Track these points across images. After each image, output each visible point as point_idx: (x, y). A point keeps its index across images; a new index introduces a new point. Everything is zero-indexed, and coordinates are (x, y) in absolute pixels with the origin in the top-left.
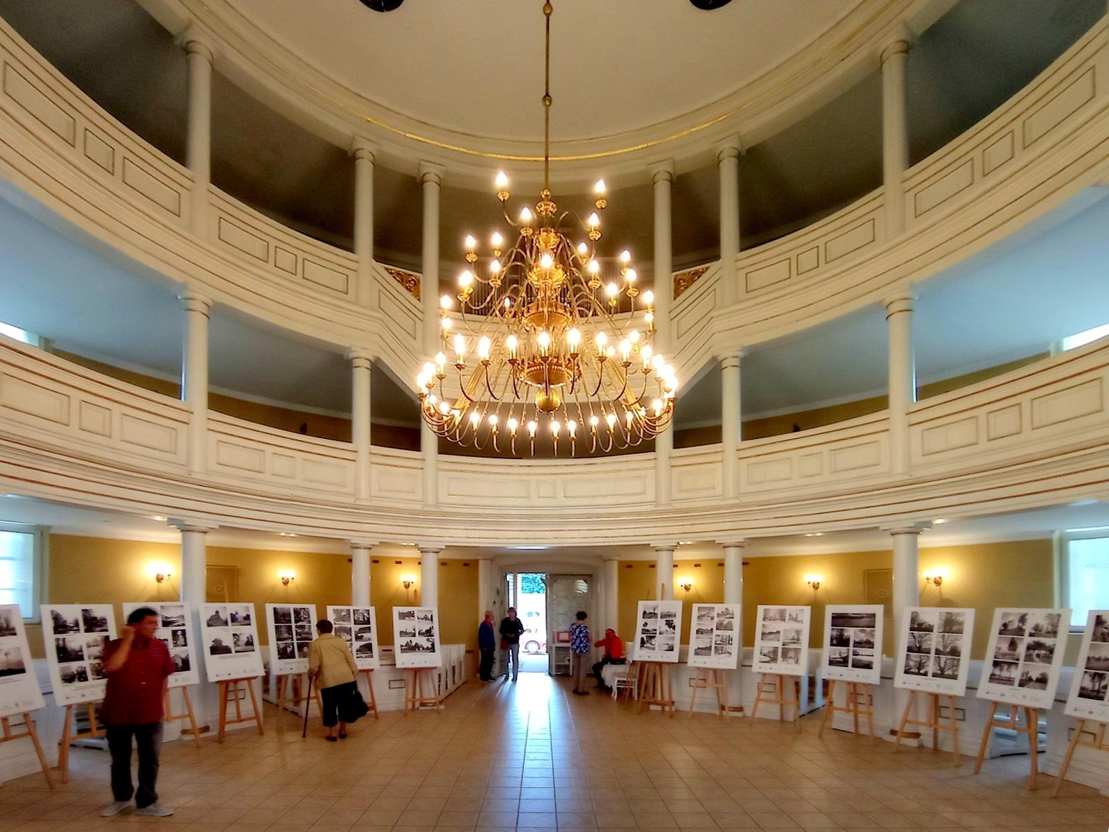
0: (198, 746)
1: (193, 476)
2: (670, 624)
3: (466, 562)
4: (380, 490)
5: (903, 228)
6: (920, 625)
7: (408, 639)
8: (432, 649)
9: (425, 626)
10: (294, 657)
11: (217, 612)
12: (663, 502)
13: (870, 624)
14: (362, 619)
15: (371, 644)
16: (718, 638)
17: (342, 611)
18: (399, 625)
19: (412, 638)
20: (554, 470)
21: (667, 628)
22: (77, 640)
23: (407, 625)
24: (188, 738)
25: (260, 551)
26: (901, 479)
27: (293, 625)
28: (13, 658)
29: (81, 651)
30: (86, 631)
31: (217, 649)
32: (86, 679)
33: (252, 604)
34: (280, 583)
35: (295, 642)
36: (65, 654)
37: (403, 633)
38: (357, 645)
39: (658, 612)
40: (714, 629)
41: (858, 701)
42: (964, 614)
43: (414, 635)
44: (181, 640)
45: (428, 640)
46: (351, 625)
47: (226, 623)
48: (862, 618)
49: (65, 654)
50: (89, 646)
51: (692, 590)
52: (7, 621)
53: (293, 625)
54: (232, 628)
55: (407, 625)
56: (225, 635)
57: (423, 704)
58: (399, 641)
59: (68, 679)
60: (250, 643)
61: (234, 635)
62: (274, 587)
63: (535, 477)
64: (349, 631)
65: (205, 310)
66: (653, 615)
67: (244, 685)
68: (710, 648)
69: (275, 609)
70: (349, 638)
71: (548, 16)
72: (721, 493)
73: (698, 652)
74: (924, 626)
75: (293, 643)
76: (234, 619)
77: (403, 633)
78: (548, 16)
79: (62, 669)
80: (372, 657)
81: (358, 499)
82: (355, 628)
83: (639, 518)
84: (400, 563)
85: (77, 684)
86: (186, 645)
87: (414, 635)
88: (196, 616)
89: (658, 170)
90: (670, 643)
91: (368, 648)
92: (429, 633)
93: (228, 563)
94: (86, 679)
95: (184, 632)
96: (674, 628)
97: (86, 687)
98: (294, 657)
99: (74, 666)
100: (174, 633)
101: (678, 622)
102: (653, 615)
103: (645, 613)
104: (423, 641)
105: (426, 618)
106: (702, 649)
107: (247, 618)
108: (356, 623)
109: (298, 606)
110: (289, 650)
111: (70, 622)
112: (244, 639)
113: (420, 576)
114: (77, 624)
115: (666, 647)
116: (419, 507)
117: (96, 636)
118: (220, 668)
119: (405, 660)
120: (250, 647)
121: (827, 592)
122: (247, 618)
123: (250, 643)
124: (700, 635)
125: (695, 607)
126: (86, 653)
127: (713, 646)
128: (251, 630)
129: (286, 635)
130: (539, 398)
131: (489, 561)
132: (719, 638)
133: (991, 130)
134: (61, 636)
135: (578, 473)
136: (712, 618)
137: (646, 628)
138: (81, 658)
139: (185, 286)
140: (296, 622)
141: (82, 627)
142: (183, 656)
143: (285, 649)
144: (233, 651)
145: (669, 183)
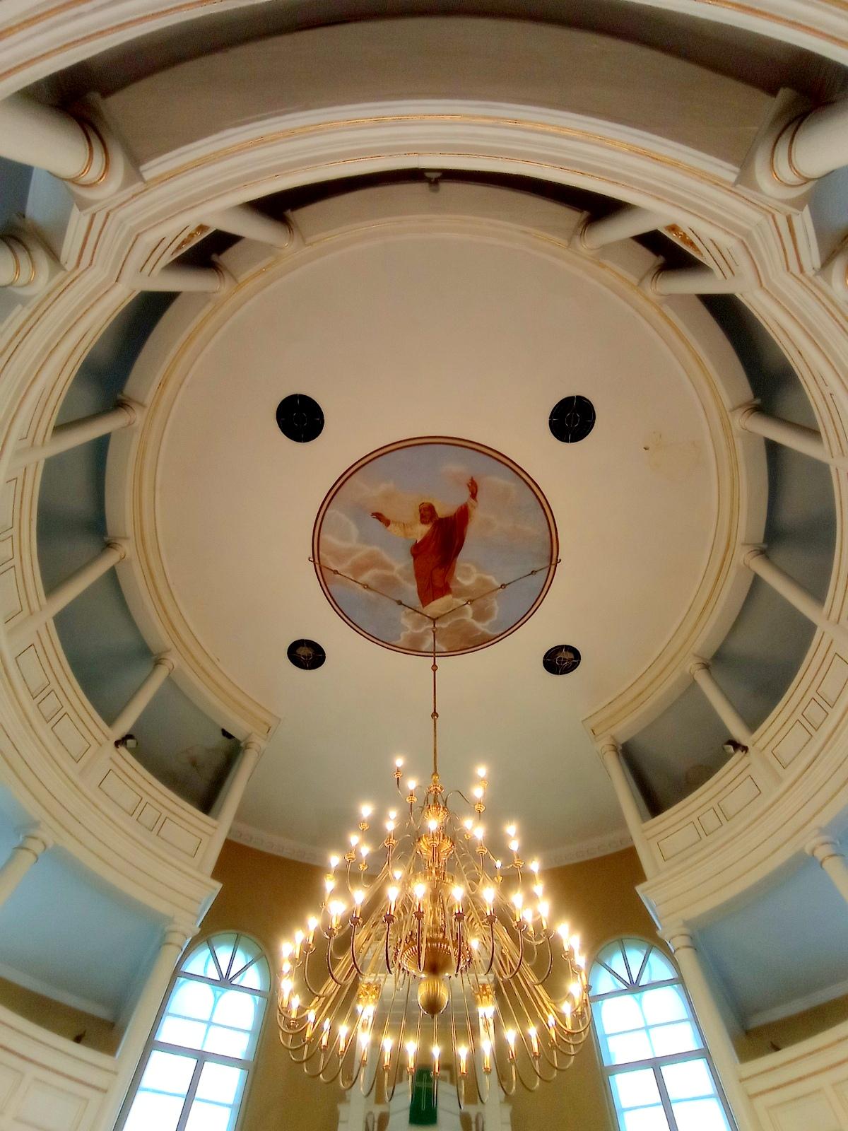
5: (779, 780)
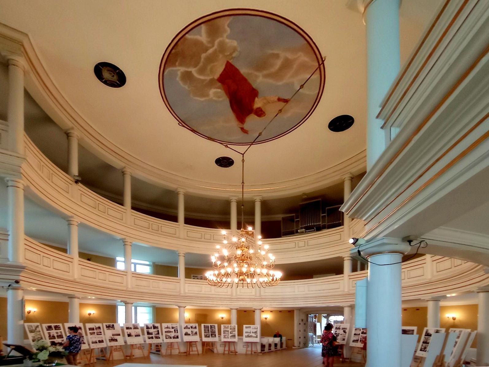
0: (180, 356)
1: (181, 295)
2: (344, 332)
3: (405, 309)
4: (240, 293)
6: (428, 334)
7: (248, 334)
8: (257, 337)
9: (255, 331)
10: (209, 337)
11: (187, 326)
12: (346, 291)
13: (412, 333)
14: (232, 328)
15: (235, 335)
16: (362, 337)
17: (226, 326)
18: (245, 330)
19: (250, 334)
20: (304, 283)
21: (343, 333)
22: (151, 331)
23: (248, 330)
24: (179, 354)
25: (214, 310)
26: (451, 274)
27: (210, 329)
28: (138, 333)
29: (152, 333)
30: (154, 329)
31: (186, 334)
32: (153, 338)
33: (217, 325)
34: (221, 318)
35: (210, 333)
36: (148, 333)
37: (246, 332)
38: (230, 335)
39: (341, 327)
40: (361, 333)
41: (197, 352)
42: (442, 330)
43: (250, 333)
44: (176, 332)
45: (255, 334)
46: (229, 329)
47: (189, 328)
48: (410, 331)
49: (148, 333)
50: (154, 332)
51: (456, 321)
52: (137, 327)
53: (210, 329)
54: (191, 330)
55: (248, 330)
56: (189, 331)
57: (231, 352)
58: (245, 334)
59: (149, 338)
60: (196, 333)
61: (192, 331)
62: (218, 320)
63: (297, 285)
64: (228, 331)
65: (183, 255)
66: (339, 328)
67: (194, 343)
68: (358, 340)
69: (204, 325)
70: (228, 333)
71: (243, 162)
72: (230, 294)
73: (354, 341)
74: (429, 334)
75: (209, 334)
76: (192, 327)
77: (246, 332)
78: (243, 162)
79: (148, 336)
80: (235, 338)
81: (232, 296)
82: (230, 331)
83: (251, 300)
84: (263, 312)
85: (151, 339)
86: (178, 333)
87: (250, 333)
88: (181, 327)
89: (345, 177)
90: (344, 338)
91: (234, 336)
92: (256, 332)
93: (204, 313)
94: (153, 338)
95: (177, 330)
96: (346, 333)
97: (153, 340)
98: (209, 337)
99: (151, 336)
100: (175, 330)
101: (347, 331)
102: (339, 328)
103: (336, 328)
104: (254, 335)
105: (255, 328)
106: (355, 340)
107: (196, 327)
108: (230, 329)
109: (211, 325)
110: (208, 335)
111: (150, 327)
112: (194, 332)
113: (261, 316)
114: (151, 327)
115: (342, 339)
116: (253, 297)
117: (156, 330)
118: (187, 339)
119: (246, 340)
120: (196, 334)
121: (460, 321)
122: (196, 327)
123: (196, 333)
124: (355, 336)
125: (222, 326)
126: (153, 333)
127: (360, 339)
128: (195, 331)
129: (207, 332)
130: (237, 270)
131: (298, 311)
132: (362, 337)
133: (138, 216)
134: (148, 330)
135: (289, 285)
136: (360, 330)
137: (336, 333)
138: (152, 334)
139: (177, 251)
140: (211, 328)
141: (152, 328)
142: (177, 335)
143: (207, 335)
144: (191, 335)
145: (350, 181)
